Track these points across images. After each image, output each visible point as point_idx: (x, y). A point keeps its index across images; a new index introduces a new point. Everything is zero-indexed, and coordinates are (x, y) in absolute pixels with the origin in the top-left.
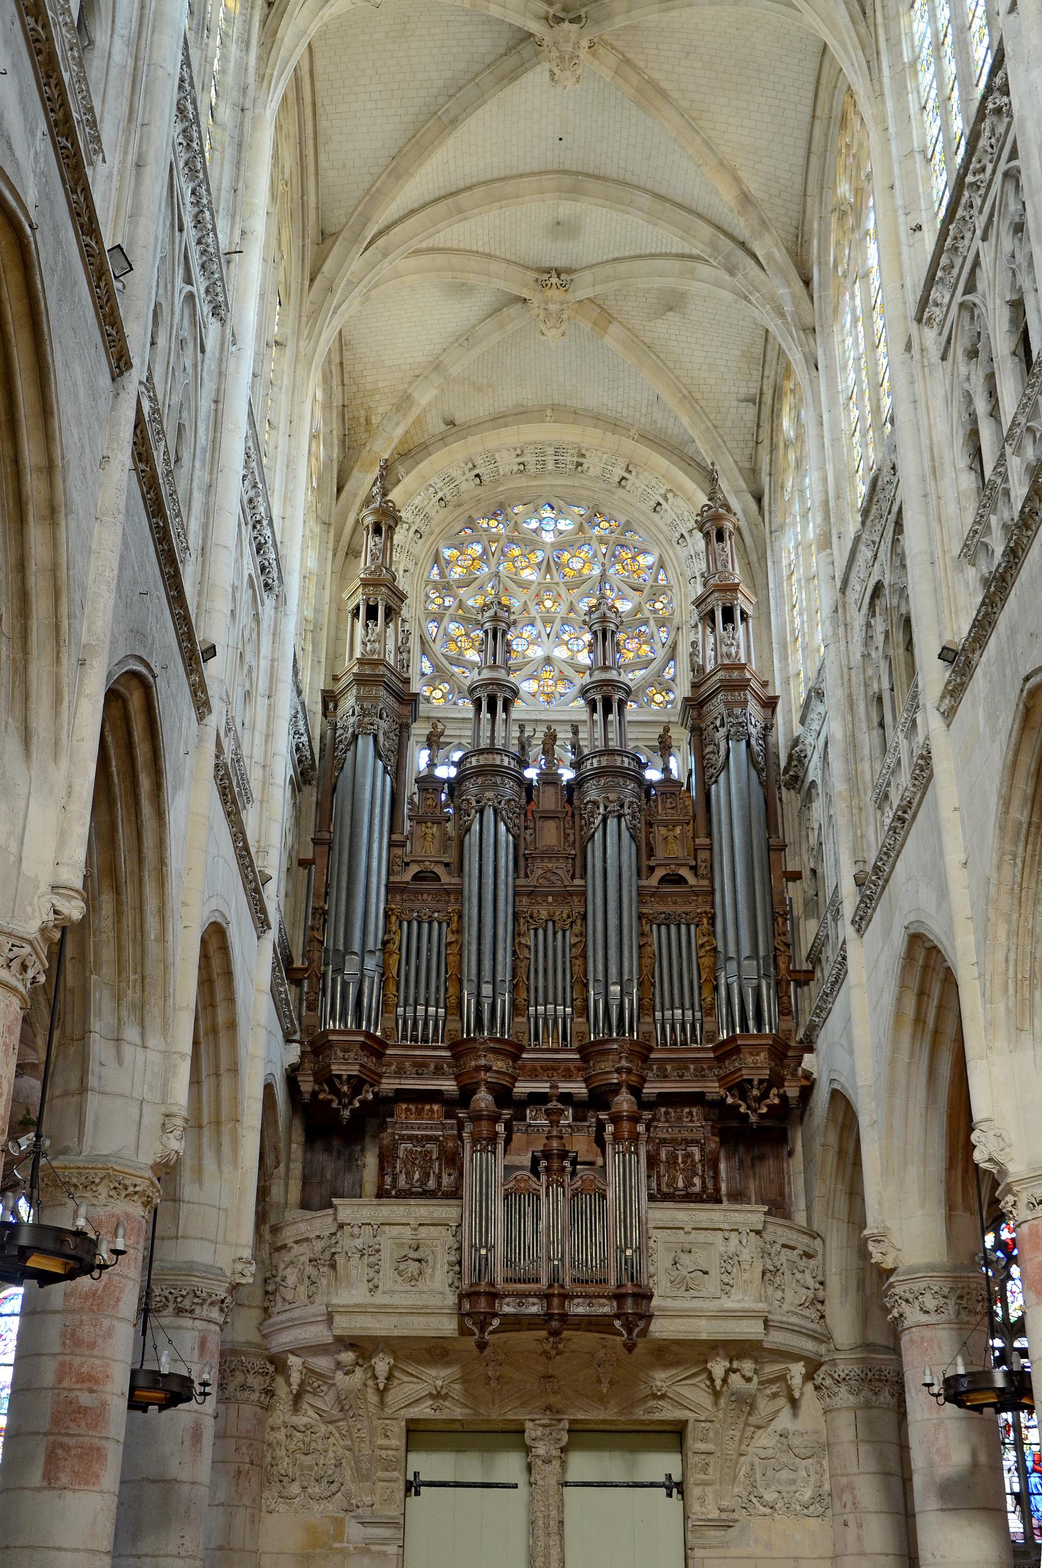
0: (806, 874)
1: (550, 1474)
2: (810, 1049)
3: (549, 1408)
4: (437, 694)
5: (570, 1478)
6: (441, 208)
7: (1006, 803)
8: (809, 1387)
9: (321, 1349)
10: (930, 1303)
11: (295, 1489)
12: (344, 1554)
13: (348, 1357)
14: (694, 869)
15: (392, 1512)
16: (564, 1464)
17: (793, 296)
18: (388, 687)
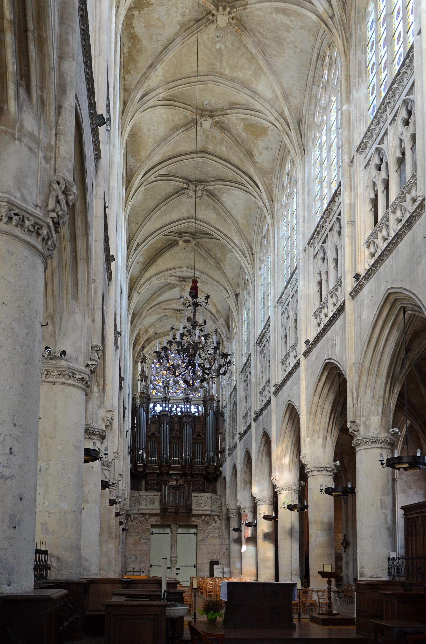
0: (223, 434)
1: (174, 533)
2: (221, 467)
3: (175, 523)
4: (154, 392)
5: (178, 532)
6: (157, 307)
7: (244, 461)
8: (218, 519)
9: (137, 514)
10: (235, 514)
11: (132, 534)
12: (141, 544)
13: (141, 516)
14: (203, 434)
15: (148, 538)
16: (177, 531)
17: (226, 331)
18: (146, 398)
